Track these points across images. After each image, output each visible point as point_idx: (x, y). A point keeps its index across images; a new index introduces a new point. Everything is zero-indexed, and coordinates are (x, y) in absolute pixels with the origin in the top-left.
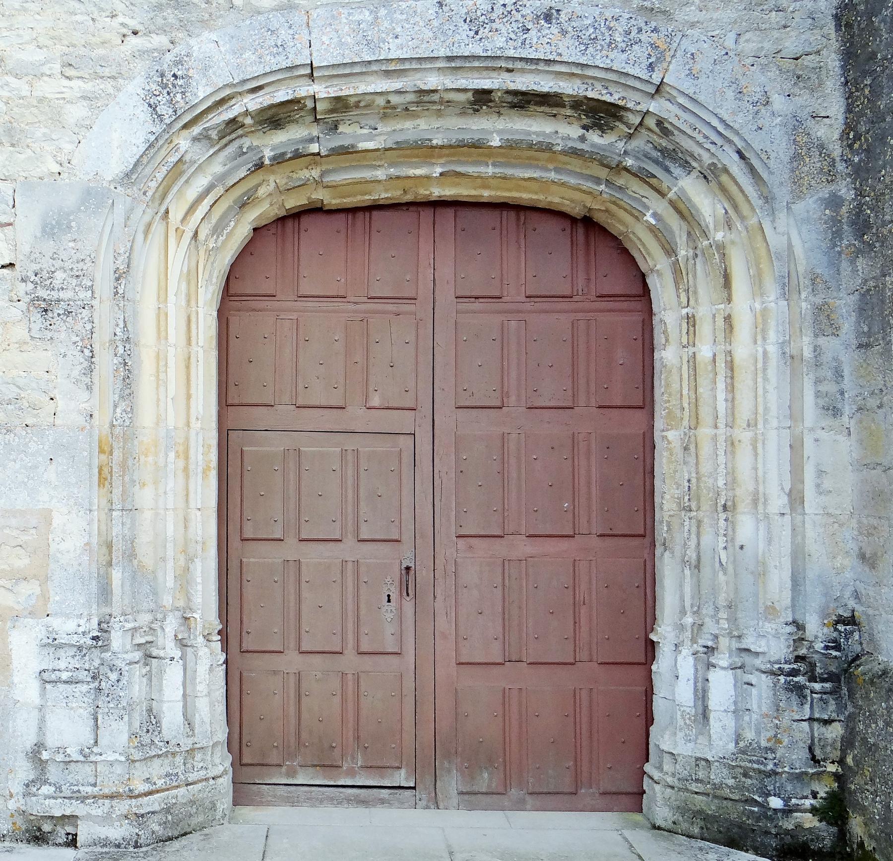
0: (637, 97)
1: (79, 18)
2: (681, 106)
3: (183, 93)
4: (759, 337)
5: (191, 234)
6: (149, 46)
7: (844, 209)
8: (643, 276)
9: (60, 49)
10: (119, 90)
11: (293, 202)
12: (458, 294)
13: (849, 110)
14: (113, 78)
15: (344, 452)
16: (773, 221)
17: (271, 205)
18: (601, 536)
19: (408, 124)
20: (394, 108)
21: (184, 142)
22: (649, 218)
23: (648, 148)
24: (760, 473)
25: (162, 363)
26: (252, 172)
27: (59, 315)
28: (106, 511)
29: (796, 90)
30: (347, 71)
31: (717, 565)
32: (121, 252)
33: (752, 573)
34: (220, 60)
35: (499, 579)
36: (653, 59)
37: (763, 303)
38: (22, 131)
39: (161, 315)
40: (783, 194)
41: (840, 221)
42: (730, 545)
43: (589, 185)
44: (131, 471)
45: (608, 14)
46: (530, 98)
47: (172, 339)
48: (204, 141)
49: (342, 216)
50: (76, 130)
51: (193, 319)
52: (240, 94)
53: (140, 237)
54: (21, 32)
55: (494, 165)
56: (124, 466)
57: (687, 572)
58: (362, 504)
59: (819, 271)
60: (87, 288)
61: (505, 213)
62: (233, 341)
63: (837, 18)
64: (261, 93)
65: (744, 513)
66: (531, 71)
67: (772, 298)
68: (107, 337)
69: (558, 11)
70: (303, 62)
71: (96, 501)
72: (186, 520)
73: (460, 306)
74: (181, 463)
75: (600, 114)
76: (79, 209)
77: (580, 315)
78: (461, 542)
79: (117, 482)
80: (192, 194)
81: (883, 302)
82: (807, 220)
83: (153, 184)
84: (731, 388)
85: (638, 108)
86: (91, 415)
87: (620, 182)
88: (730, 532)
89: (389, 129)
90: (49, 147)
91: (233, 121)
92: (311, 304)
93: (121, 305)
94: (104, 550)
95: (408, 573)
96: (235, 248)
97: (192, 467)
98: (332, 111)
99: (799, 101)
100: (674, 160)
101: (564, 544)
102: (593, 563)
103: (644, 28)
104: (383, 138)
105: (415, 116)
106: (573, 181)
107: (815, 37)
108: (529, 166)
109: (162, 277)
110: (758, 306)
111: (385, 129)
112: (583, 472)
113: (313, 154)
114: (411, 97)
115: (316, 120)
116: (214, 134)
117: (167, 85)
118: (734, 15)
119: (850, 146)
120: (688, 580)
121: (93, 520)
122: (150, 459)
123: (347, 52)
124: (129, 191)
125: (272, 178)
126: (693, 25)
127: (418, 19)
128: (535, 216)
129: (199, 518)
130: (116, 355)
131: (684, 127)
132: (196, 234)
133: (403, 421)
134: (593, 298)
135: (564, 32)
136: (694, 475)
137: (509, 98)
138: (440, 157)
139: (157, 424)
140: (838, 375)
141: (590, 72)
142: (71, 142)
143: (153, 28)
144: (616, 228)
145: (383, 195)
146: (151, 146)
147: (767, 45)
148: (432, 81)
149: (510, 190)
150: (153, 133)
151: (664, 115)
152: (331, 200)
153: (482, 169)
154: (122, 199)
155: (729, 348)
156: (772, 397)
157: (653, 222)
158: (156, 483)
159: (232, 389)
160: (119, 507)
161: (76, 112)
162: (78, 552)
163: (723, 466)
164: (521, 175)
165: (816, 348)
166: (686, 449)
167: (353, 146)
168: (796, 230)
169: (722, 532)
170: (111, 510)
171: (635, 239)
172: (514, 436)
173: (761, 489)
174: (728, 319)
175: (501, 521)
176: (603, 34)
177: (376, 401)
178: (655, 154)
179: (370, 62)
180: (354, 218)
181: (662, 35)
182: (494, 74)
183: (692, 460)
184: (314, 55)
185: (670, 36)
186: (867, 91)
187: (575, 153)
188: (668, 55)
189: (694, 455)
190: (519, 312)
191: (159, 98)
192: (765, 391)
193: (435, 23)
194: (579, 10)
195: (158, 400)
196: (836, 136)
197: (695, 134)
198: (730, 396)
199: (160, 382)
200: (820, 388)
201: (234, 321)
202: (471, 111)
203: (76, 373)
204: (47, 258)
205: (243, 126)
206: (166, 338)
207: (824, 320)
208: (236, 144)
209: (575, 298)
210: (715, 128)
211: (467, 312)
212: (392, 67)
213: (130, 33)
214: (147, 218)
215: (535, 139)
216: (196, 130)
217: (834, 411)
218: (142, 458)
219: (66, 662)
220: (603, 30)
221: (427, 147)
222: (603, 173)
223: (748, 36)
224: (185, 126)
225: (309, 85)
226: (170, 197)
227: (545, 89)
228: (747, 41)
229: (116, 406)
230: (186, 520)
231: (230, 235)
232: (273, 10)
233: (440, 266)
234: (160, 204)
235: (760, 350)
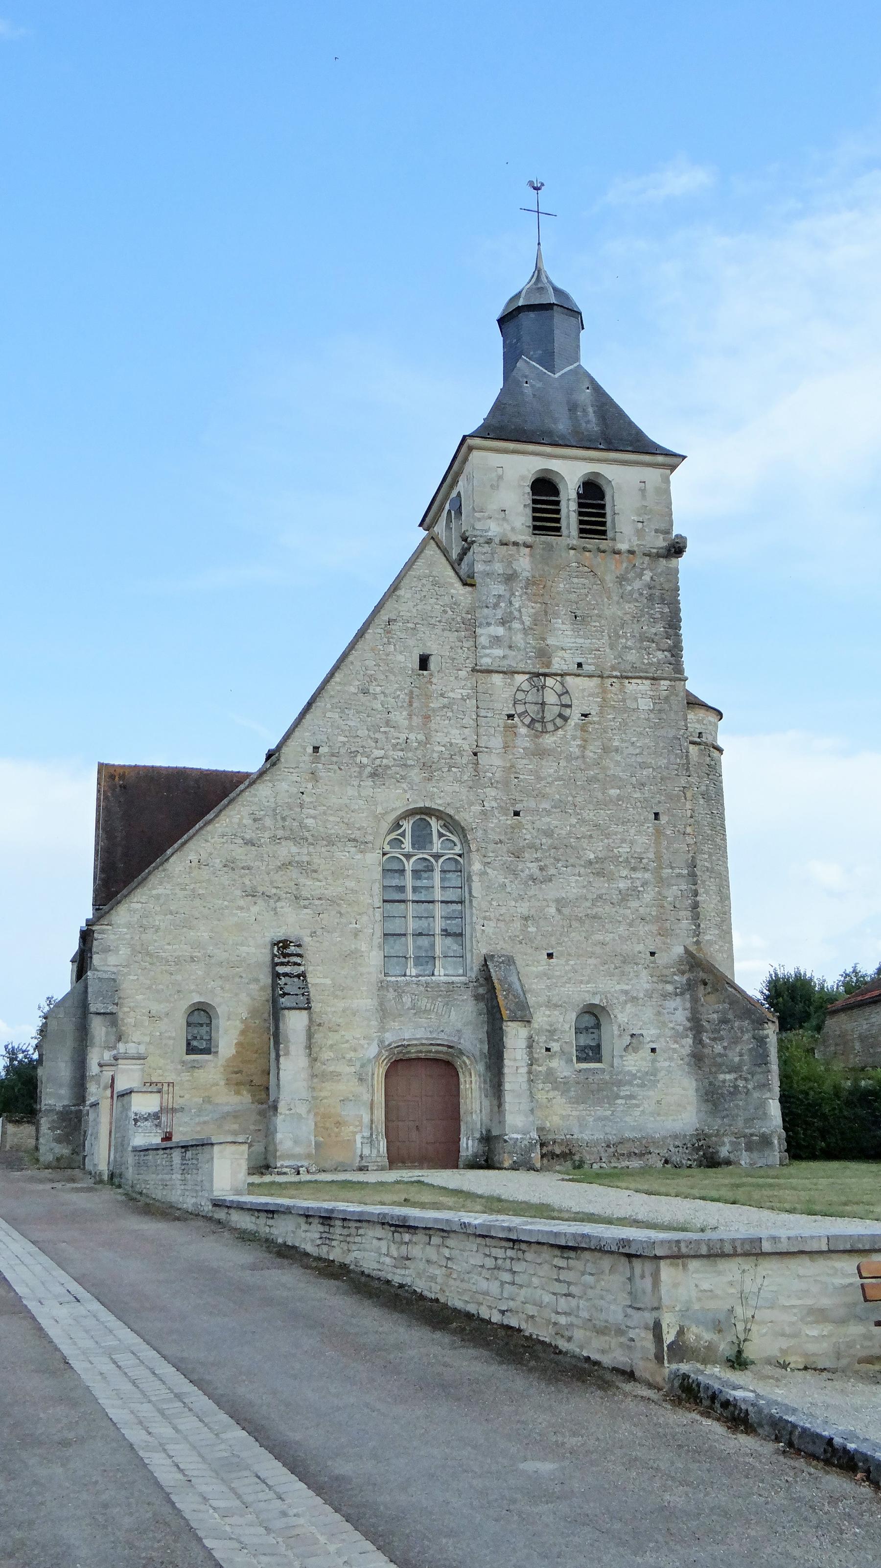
34: (389, 1038)
168: (481, 1067)
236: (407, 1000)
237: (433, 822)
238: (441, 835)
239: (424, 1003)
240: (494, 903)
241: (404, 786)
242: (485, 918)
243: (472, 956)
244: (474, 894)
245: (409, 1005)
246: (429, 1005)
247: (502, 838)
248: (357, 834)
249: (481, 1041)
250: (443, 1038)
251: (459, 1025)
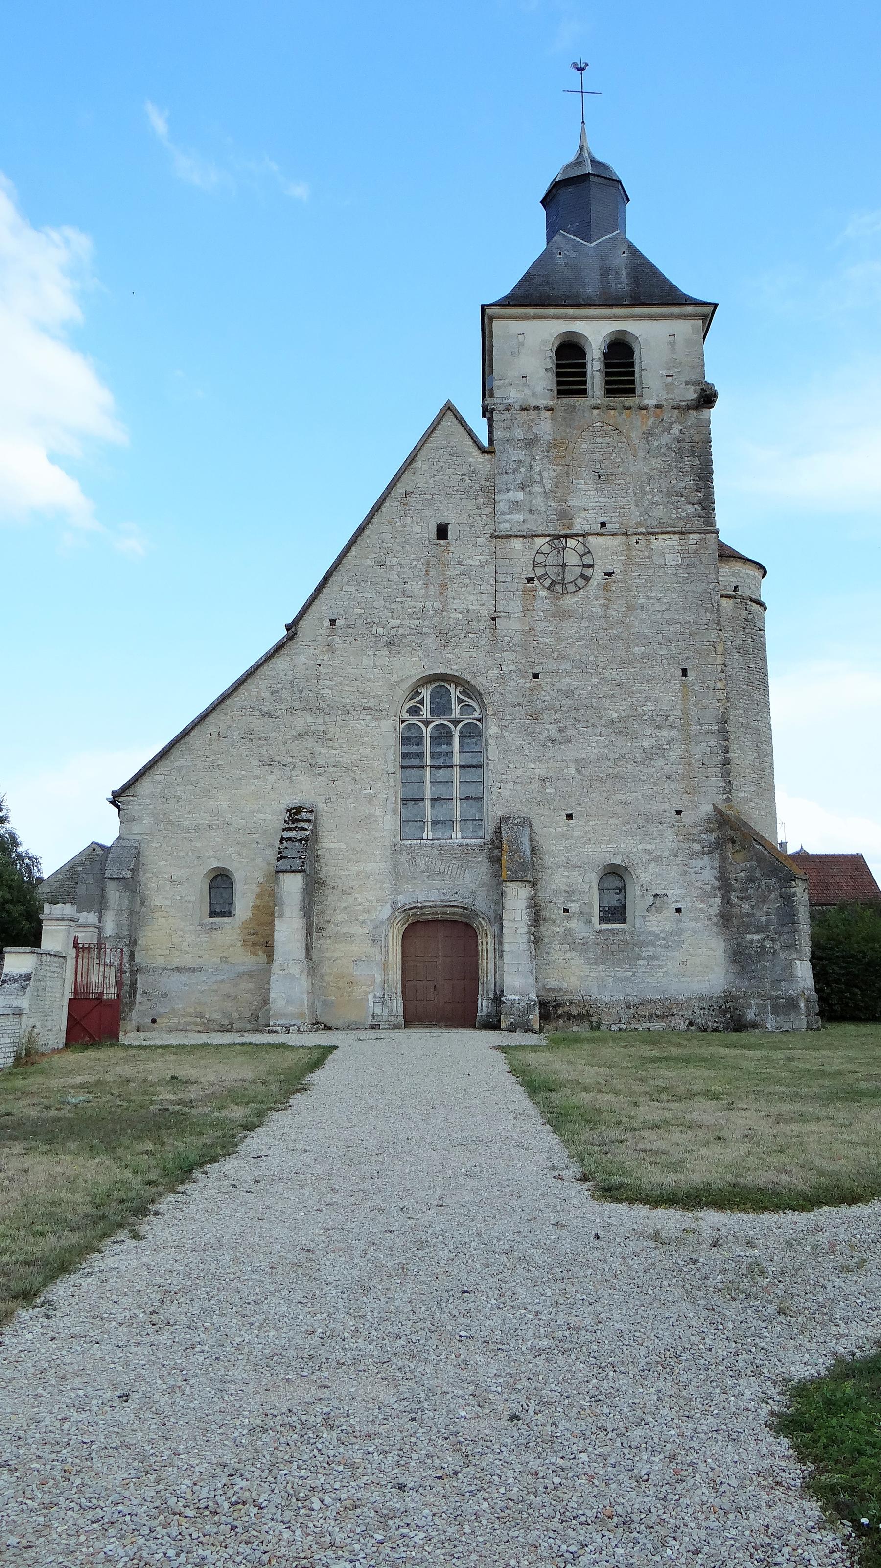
161: (379, 908)
219: (377, 1000)
237: (452, 688)
238: (460, 701)
241: (420, 653)
242: (501, 781)
245: (423, 867)
247: (521, 700)
248: (372, 703)
250: (457, 900)
251: (473, 887)
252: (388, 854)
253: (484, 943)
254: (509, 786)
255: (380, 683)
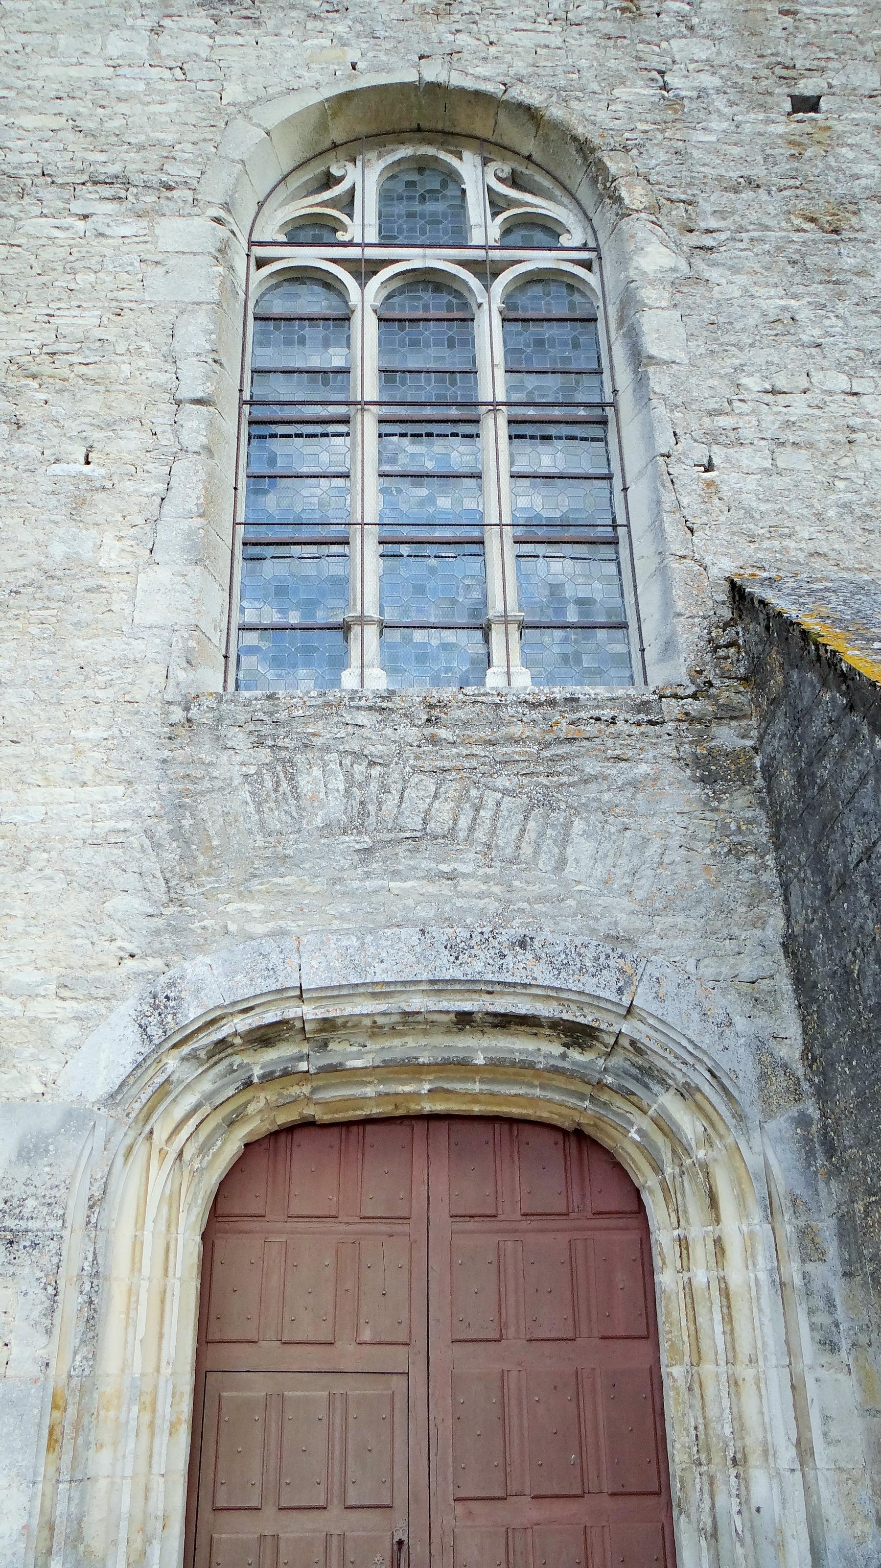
0: (611, 1018)
1: (79, 941)
2: (651, 1026)
3: (174, 1014)
4: (750, 1262)
5: (175, 1155)
6: (145, 968)
7: (814, 1129)
8: (638, 1192)
9: (57, 970)
10: (111, 1011)
11: (284, 1118)
12: (454, 1213)
13: (805, 1032)
14: (107, 999)
15: (331, 1397)
16: (748, 1141)
17: (262, 1121)
18: (613, 1494)
19: (397, 1042)
20: (381, 1027)
21: (172, 1063)
22: (633, 1134)
23: (627, 1065)
24: (767, 1420)
25: (133, 1299)
26: (240, 1091)
27: (25, 1247)
28: (54, 1481)
29: (756, 1012)
30: (335, 993)
31: (734, 1533)
32: (98, 1177)
33: (772, 1542)
34: (211, 983)
35: (503, 1556)
36: (621, 983)
37: (749, 1225)
38: (10, 1051)
39: (137, 1243)
40: (754, 1113)
41: (812, 1140)
42: (744, 1508)
43: (572, 1101)
44: (86, 1430)
45: (578, 941)
46: (509, 1019)
47: (146, 1272)
48: (193, 1061)
49: (335, 1131)
50: (65, 1050)
51: (172, 1247)
52: (232, 1014)
53: (120, 1160)
54: (21, 954)
55: (482, 1081)
56: (77, 1426)
57: (703, 1543)
58: (350, 1459)
59: (798, 1192)
60: (57, 1218)
61: (497, 1126)
62: (217, 1267)
63: (783, 945)
64: (252, 1013)
65: (756, 1467)
66: (509, 994)
67: (756, 1221)
68: (75, 1271)
69: (532, 939)
70: (292, 985)
71: (42, 1469)
72: (147, 1489)
73: (455, 1227)
74: (146, 1418)
75: (578, 1035)
76: (59, 1132)
77: (577, 1235)
78: (460, 1508)
79: (68, 1447)
80: (179, 1112)
81: (856, 1230)
82: (781, 1140)
83: (137, 1106)
84: (728, 1319)
85: (611, 1029)
86: (47, 1364)
87: (604, 1097)
88: (743, 1492)
89: (378, 1047)
90: (35, 1068)
91: (222, 1041)
92: (301, 1225)
93: (93, 1236)
94: (46, 1533)
95: (400, 1549)
96: (223, 1167)
97: (158, 1422)
98: (321, 1031)
99: (759, 1022)
100: (652, 1077)
101: (572, 1508)
102: (606, 1530)
103: (612, 954)
104: (371, 1056)
105: (401, 1034)
106: (557, 1097)
107: (767, 963)
108: (516, 1082)
109: (142, 1201)
110: (745, 1228)
111: (374, 1047)
112: (589, 1415)
113: (304, 1072)
114: (396, 1018)
115: (306, 1039)
116: (202, 1054)
117: (158, 1006)
118: (692, 943)
119: (811, 1067)
120: (705, 1553)
121: (36, 1494)
122: (112, 1414)
123: (335, 975)
124: (112, 1113)
125: (262, 1095)
126: (656, 952)
127: (402, 945)
128: (528, 1129)
129: (162, 1487)
130: (81, 1292)
131: (656, 1048)
132: (180, 1154)
133: (397, 1358)
134: (590, 1215)
135: (538, 958)
136: (700, 1421)
137: (491, 1019)
138: (429, 1073)
139: (123, 1370)
140: (831, 1304)
141: (564, 995)
142: (59, 1062)
143: (149, 951)
144: (607, 1143)
145: (375, 1111)
146: (139, 1066)
147: (724, 970)
148: (417, 1003)
149: (499, 1104)
150: (140, 1053)
151: (636, 1036)
152: (322, 1116)
153: (469, 1086)
154: (104, 1120)
155: (722, 1274)
156: (768, 1329)
157: (638, 1139)
158: (115, 1444)
159: (214, 1325)
160: (68, 1478)
161: (66, 1032)
162: (14, 1537)
163: (728, 1411)
164: (507, 1092)
165: (805, 1275)
166: (690, 1389)
167: (341, 1064)
168: (770, 1148)
169: (734, 1492)
170: (58, 1481)
171: (624, 1154)
172: (514, 1374)
173: (769, 1437)
174: (718, 1242)
175: (503, 1478)
176: (574, 960)
177: (366, 1335)
178: (634, 1071)
179: (357, 985)
180: (348, 1132)
181: (628, 961)
182: (475, 996)
183: (698, 1403)
184: (303, 978)
185: (635, 961)
186: (815, 1016)
187: (556, 1070)
188: (635, 979)
189: (699, 1397)
190: (515, 1231)
191: (150, 1019)
192: (761, 1324)
193: (418, 949)
194: (550, 939)
195: (126, 1342)
196: (798, 1056)
197: (666, 1055)
198: (728, 1328)
199: (130, 1322)
200: (814, 1320)
201: (219, 1243)
202: (455, 1030)
203: (35, 1314)
204: (20, 1183)
205: (232, 1045)
206: (140, 1271)
207: (808, 1244)
208: (226, 1062)
209: (572, 1216)
210: (685, 1048)
211: (463, 1232)
212: (378, 989)
213: (127, 955)
214: (128, 1141)
215: (518, 1057)
216: (185, 1050)
217: (832, 1347)
218: (102, 1413)
220: (574, 955)
221: (414, 1064)
222: (587, 1090)
223: (707, 961)
224: (175, 1046)
225: (298, 1007)
226: (155, 1116)
227: (523, 1011)
228: (706, 966)
229: (75, 1353)
230: (147, 1489)
231: (215, 1155)
232: (265, 936)
233: (437, 1184)
234: (144, 1126)
235: (752, 1276)
236: (324, 787)
237: (472, 172)
238: (496, 204)
239: (419, 800)
240: (753, 383)
241: (341, 29)
242: (712, 438)
243: (666, 592)
244: (652, 346)
245: (335, 807)
246: (443, 811)
247: (759, 172)
248: (130, 162)
249: (759, 1001)
250: (534, 980)
251: (622, 915)
252: (144, 743)
253: (700, 1252)
254: (753, 458)
255: (171, 107)
